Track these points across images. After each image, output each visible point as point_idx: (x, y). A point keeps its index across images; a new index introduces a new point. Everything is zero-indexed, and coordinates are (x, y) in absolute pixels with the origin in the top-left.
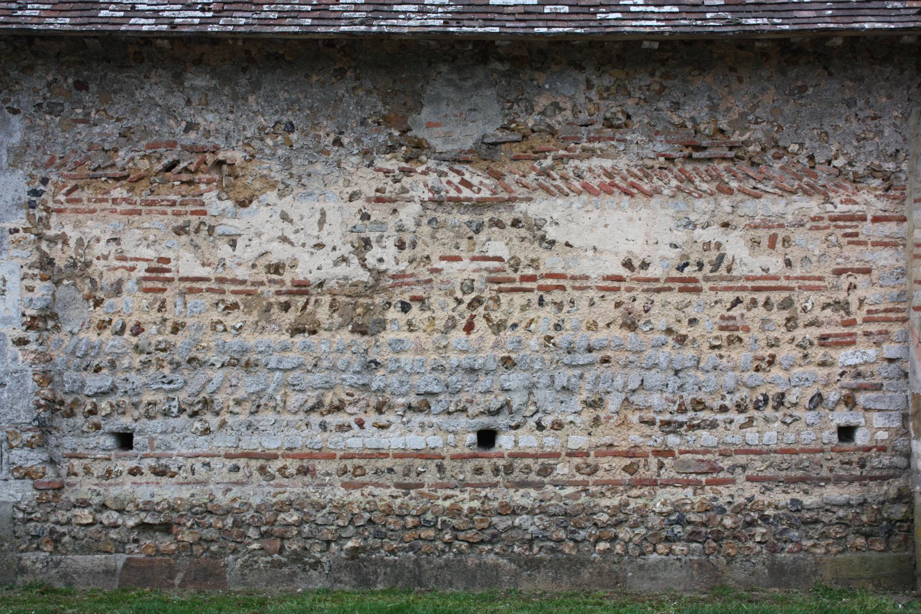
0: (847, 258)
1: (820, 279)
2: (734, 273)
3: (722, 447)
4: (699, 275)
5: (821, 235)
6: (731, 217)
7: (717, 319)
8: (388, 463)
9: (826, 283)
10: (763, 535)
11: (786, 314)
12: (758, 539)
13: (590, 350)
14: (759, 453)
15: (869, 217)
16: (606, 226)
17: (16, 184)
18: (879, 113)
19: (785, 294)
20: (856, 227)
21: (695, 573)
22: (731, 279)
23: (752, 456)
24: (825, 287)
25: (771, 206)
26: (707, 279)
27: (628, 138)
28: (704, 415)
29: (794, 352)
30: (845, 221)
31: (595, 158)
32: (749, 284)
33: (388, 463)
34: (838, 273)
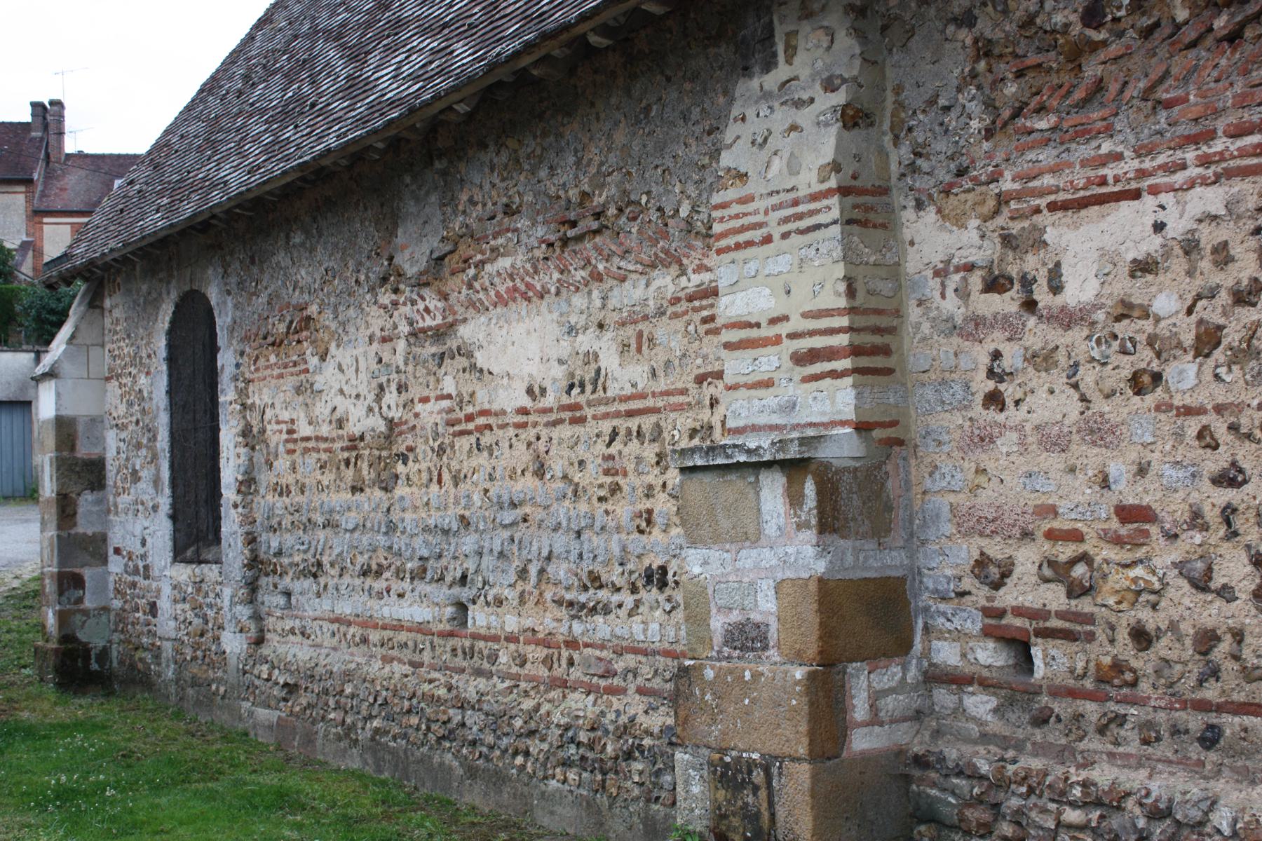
0: (705, 357)
1: (684, 392)
2: (610, 394)
3: (616, 642)
4: (582, 400)
5: (679, 324)
6: (603, 313)
7: (599, 460)
8: (403, 636)
9: (690, 399)
10: (641, 773)
11: (656, 447)
12: (636, 779)
13: (514, 505)
14: (645, 653)
15: (433, 401)
16: (513, 344)
17: (858, 3)
18: (715, 123)
19: (653, 419)
20: (712, 306)
21: (584, 814)
22: (607, 402)
23: (640, 658)
24: (689, 404)
25: (633, 293)
26: (589, 404)
27: (519, 225)
28: (603, 594)
29: (669, 505)
30: (701, 298)
31: (500, 259)
32: (623, 407)
33: (403, 636)
34: (700, 380)
